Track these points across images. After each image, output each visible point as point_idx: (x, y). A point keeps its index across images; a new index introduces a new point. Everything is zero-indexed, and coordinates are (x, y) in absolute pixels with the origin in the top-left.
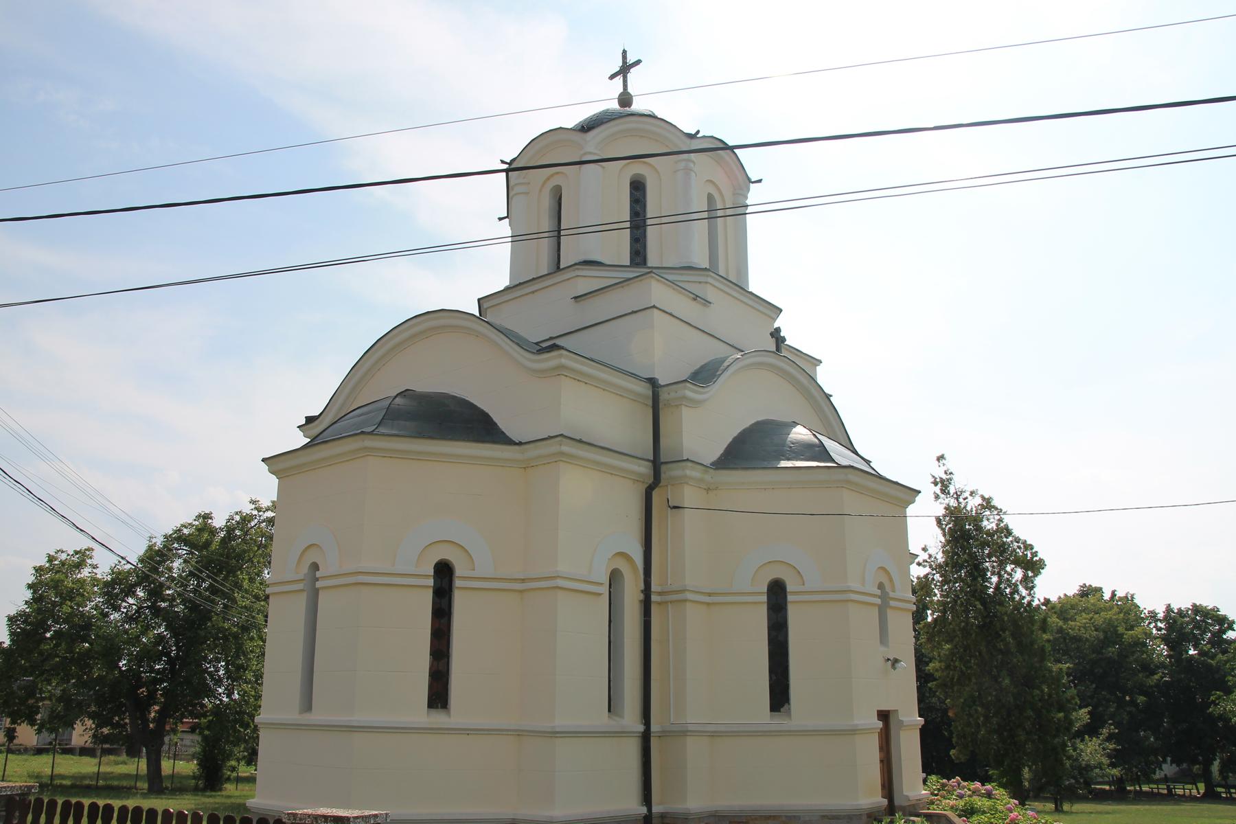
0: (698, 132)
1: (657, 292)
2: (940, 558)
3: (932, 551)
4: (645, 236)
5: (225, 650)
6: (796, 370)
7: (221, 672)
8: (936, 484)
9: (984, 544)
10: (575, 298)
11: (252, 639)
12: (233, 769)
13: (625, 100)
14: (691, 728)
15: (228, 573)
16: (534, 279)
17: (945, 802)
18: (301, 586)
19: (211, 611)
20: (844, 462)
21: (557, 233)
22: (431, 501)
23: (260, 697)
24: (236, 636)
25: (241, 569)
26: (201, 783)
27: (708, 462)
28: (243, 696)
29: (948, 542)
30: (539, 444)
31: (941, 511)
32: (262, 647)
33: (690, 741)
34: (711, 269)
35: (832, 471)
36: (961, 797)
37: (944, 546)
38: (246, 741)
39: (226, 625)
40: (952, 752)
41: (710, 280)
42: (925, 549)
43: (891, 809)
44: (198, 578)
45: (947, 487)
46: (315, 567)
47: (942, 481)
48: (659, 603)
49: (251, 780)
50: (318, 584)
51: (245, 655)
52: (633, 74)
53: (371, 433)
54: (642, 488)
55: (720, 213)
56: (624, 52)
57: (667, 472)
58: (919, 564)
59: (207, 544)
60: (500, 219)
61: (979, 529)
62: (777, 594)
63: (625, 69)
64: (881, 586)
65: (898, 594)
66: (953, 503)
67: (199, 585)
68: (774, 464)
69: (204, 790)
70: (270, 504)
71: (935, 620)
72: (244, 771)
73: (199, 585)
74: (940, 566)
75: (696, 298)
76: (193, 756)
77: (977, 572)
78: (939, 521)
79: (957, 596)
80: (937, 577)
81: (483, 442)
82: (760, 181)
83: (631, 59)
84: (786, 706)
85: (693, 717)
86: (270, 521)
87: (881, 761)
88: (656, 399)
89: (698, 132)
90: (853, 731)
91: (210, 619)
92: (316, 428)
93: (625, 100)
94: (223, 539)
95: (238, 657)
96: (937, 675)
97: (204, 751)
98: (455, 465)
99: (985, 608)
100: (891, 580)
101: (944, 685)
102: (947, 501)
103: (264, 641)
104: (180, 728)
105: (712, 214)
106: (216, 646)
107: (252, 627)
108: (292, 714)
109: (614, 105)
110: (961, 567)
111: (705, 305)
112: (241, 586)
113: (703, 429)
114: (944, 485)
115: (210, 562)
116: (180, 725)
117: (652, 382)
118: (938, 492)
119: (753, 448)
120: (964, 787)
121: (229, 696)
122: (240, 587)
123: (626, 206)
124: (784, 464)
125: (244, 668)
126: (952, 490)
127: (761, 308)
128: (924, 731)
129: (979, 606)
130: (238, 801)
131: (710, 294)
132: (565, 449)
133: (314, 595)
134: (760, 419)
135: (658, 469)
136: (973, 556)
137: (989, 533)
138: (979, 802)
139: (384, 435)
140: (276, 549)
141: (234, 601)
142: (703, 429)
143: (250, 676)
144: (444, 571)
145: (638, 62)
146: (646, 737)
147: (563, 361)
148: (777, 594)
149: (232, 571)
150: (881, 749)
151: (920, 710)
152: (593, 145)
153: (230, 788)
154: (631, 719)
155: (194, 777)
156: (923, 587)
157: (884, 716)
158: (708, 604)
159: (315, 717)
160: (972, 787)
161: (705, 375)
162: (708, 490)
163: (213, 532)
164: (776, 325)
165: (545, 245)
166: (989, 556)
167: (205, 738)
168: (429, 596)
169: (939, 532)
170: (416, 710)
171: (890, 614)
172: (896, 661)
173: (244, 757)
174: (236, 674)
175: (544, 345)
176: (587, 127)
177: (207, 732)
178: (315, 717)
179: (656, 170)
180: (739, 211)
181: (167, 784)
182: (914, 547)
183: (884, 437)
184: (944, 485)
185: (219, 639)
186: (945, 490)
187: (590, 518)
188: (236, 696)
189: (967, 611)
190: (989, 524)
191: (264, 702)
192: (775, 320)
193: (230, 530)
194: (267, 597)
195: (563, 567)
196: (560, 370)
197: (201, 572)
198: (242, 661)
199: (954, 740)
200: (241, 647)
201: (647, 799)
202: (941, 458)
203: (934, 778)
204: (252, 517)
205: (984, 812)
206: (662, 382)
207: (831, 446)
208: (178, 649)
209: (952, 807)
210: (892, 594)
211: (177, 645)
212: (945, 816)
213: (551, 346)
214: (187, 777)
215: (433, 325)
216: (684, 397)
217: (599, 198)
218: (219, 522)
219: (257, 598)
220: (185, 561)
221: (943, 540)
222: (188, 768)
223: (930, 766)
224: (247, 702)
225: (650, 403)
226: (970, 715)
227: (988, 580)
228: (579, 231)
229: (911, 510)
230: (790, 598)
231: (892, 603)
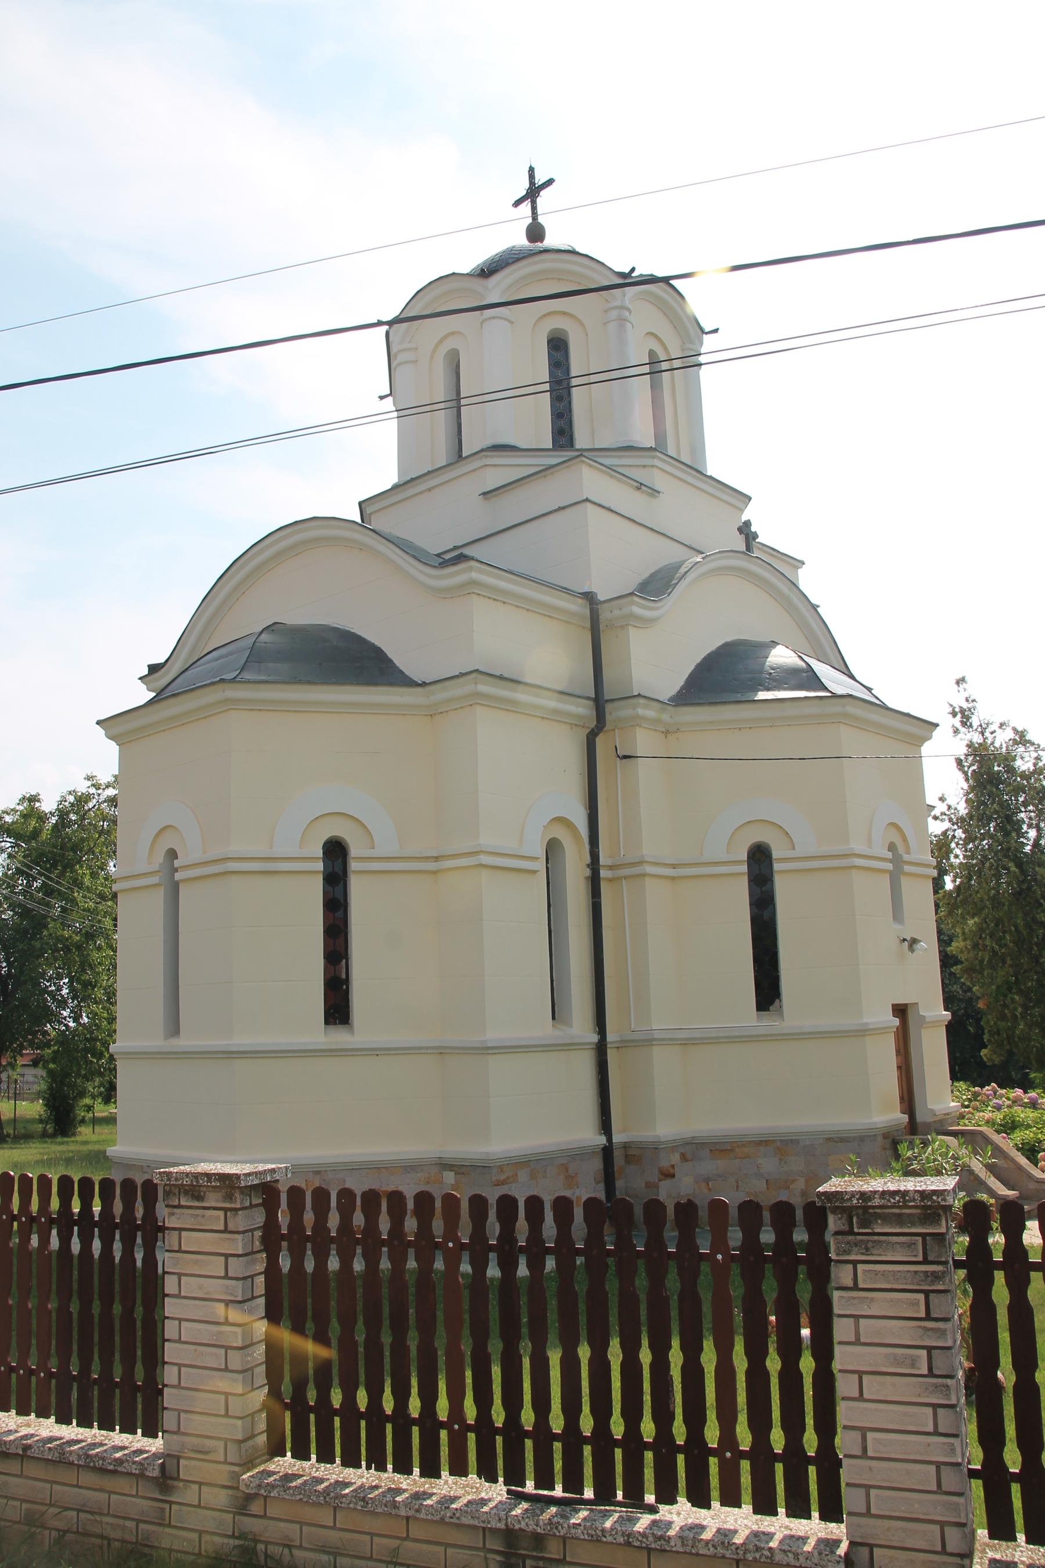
0: (633, 270)
1: (590, 481)
2: (963, 810)
3: (952, 801)
4: (570, 410)
5: (67, 963)
6: (769, 571)
7: (65, 991)
8: (954, 714)
9: (1019, 789)
10: (484, 494)
11: (99, 948)
12: (89, 1108)
13: (536, 232)
14: (657, 1035)
15: (65, 868)
16: (429, 472)
17: (978, 1115)
18: (155, 879)
19: (45, 917)
20: (840, 690)
21: (456, 403)
22: (310, 767)
23: (115, 1019)
24: (79, 947)
25: (79, 861)
26: (50, 1128)
27: (665, 697)
28: (93, 1019)
29: (972, 788)
30: (447, 683)
31: (962, 750)
32: (113, 958)
33: (657, 1051)
34: (658, 448)
35: (825, 701)
36: (998, 1108)
37: (967, 794)
38: (101, 1074)
39: (66, 934)
40: (984, 1052)
42: (942, 799)
43: (913, 1127)
44: (28, 876)
45: (968, 718)
46: (172, 854)
47: (962, 711)
48: (610, 880)
49: (111, 1120)
50: (178, 876)
51: (92, 968)
52: (544, 199)
53: (233, 680)
54: (583, 734)
55: (665, 366)
56: (531, 170)
57: (612, 712)
58: (936, 818)
59: (36, 834)
60: (381, 398)
61: (1011, 770)
62: (760, 862)
63: (533, 193)
64: (892, 847)
65: (914, 857)
66: (977, 739)
67: (29, 885)
68: (749, 696)
69: (54, 1135)
70: (111, 779)
71: (958, 889)
72: (101, 1110)
73: (29, 885)
74: (962, 819)
75: (640, 486)
76: (39, 1095)
77: (1010, 825)
78: (959, 762)
79: (985, 857)
80: (959, 833)
81: (376, 684)
82: (716, 331)
83: (540, 179)
84: (777, 1001)
85: (660, 1022)
86: (113, 801)
87: (899, 1068)
88: (597, 624)
89: (633, 270)
90: (863, 1032)
91: (45, 926)
92: (163, 679)
93: (536, 232)
94: (55, 826)
95: (84, 971)
96: (962, 957)
97: (50, 1088)
98: (334, 719)
99: (1022, 871)
100: (905, 839)
101: (970, 970)
102: (969, 736)
103: (115, 951)
104: (20, 1061)
105: (654, 367)
106: (56, 959)
107: (97, 934)
108: (157, 1042)
109: (520, 240)
110: (990, 820)
111: (651, 495)
112: (82, 884)
113: (658, 657)
114: (965, 716)
115: (41, 855)
116: (18, 1058)
117: (589, 597)
118: (958, 725)
119: (724, 676)
120: (1001, 1096)
121: (76, 1020)
122: (78, 883)
123: (551, 365)
124: (762, 695)
125: (92, 984)
126: (975, 721)
127: (724, 497)
128: (950, 1028)
129: (1013, 868)
130: (97, 1147)
131: (659, 480)
132: (482, 688)
133: (174, 889)
134: (729, 639)
136: (1004, 805)
137: (1024, 776)
138: (1023, 1114)
139: (249, 682)
140: (121, 836)
141: (73, 901)
143: (99, 993)
144: (336, 852)
145: (550, 182)
146: (601, 1049)
147: (474, 575)
148: (760, 862)
149: (69, 866)
150: (898, 1052)
151: (945, 1000)
152: (495, 289)
153: (85, 1132)
154: (580, 1026)
155: (41, 1121)
156: (942, 846)
157: (901, 1011)
158: (673, 878)
159: (185, 1042)
160: (1012, 1095)
161: (658, 585)
162: (667, 733)
163: (42, 817)
164: (744, 518)
165: (441, 419)
166: (1025, 804)
167: (51, 1073)
168: (318, 883)
169: (960, 776)
170: (313, 1030)
171: (905, 883)
172: (914, 941)
173: (101, 1094)
174: (83, 990)
175: (447, 557)
176: (487, 271)
177: (52, 1066)
178: (185, 1042)
179: (582, 324)
180: (691, 363)
181: (8, 1130)
182: (931, 799)
183: (888, 658)
184: (965, 716)
185: (58, 951)
186: (966, 722)
187: (519, 780)
188: (85, 1020)
189: (998, 876)
190: (1024, 764)
191: (119, 1025)
192: (742, 511)
193: (63, 814)
194: (115, 896)
195: (487, 839)
196: (470, 588)
197: (31, 868)
198: (88, 976)
199: (986, 1037)
200: (87, 958)
201: (606, 1126)
203: (962, 1085)
204: (88, 797)
205: (1028, 1127)
206: (601, 597)
207: (822, 670)
208: (10, 965)
209: (988, 1122)
210: (906, 857)
211: (7, 960)
212: (981, 1133)
213: (457, 558)
214: (32, 1121)
215: (299, 541)
216: (632, 616)
217: (507, 355)
218: (48, 805)
219: (102, 897)
220: (10, 856)
221: (965, 786)
222: (32, 1109)
223: (965, 1067)
224: (98, 1027)
225: (588, 624)
226: (1005, 1006)
227: (1023, 835)
228: (486, 398)
229: (926, 749)
230: (776, 866)
231: (907, 868)
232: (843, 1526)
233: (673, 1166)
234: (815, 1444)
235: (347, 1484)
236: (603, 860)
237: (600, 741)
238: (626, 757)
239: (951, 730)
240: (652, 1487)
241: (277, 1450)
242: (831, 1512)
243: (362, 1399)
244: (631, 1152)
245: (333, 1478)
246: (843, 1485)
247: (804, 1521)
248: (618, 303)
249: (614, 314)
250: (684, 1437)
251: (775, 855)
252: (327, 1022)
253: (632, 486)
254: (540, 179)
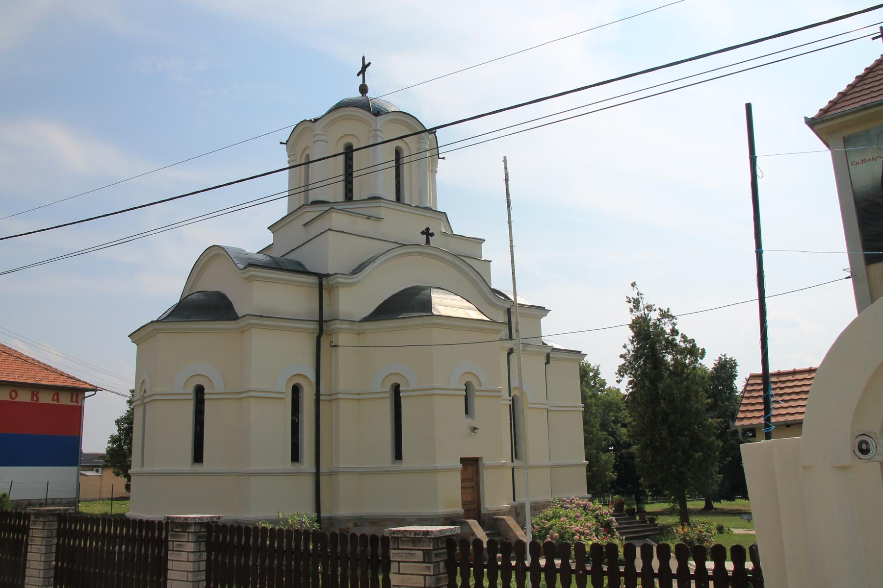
22: (203, 353)
54: (315, 336)
56: (364, 58)
63: (363, 71)
85: (343, 465)
93: (363, 89)
98: (209, 335)
113: (356, 300)
123: (364, 157)
132: (251, 321)
135: (322, 326)
142: (356, 300)
144: (199, 391)
146: (317, 475)
147: (251, 273)
159: (146, 469)
202: (633, 285)
216: (338, 283)
236: (322, 391)
251: (205, 391)
254: (366, 63)
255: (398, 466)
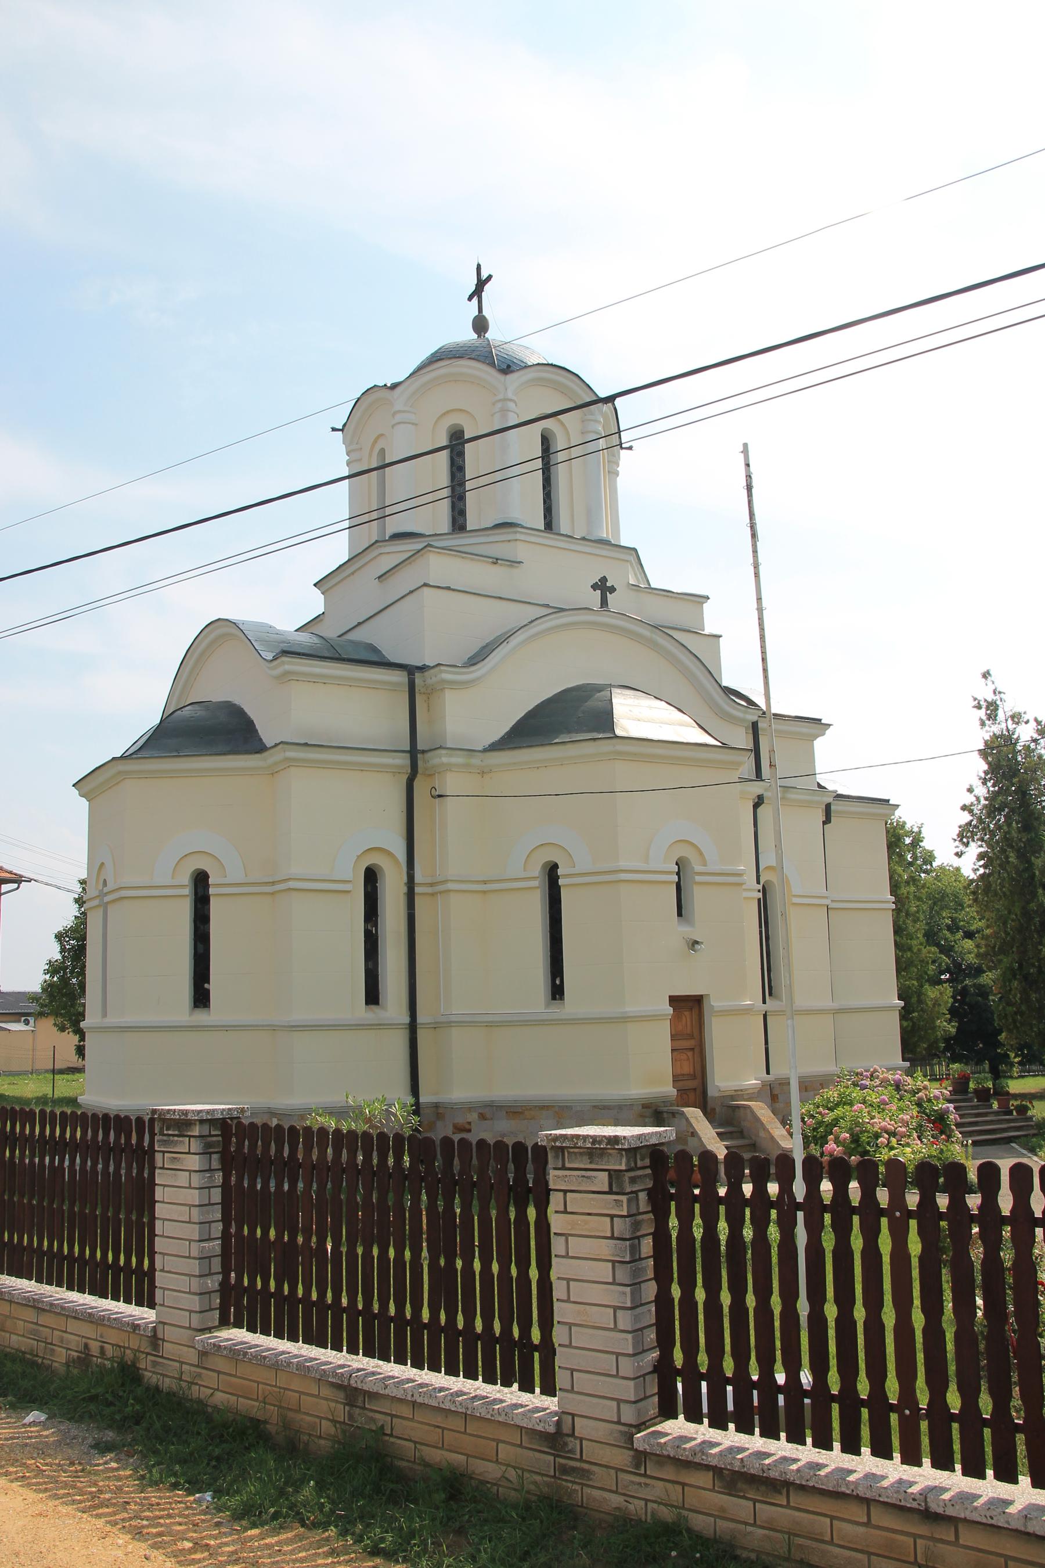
14: (453, 1018)
33: (455, 1033)
41: (518, 536)
54: (404, 778)
56: (479, 267)
60: (334, 429)
63: (481, 284)
83: (484, 275)
93: (480, 325)
118: (984, 718)
123: (484, 451)
135: (415, 760)
144: (201, 880)
146: (413, 1027)
147: (287, 667)
158: (484, 892)
170: (360, 1010)
201: (415, 1090)
202: (986, 675)
216: (444, 681)
231: (698, 878)
232: (556, 1399)
233: (469, 1123)
234: (990, 1408)
235: (769, 1455)
236: (418, 878)
237: (417, 784)
238: (440, 796)
239: (978, 723)
240: (959, 1461)
241: (668, 1412)
242: (549, 1390)
243: (986, 1404)
244: (441, 1111)
245: (781, 1454)
246: (557, 1368)
247: (946, 1473)
248: (501, 397)
249: (499, 405)
250: (867, 1393)
252: (367, 1003)
253: (488, 562)
254: (484, 275)
255: (557, 1011)
